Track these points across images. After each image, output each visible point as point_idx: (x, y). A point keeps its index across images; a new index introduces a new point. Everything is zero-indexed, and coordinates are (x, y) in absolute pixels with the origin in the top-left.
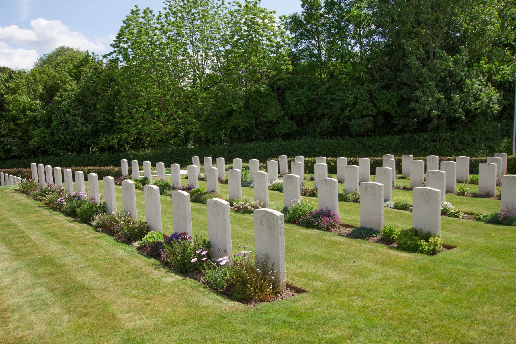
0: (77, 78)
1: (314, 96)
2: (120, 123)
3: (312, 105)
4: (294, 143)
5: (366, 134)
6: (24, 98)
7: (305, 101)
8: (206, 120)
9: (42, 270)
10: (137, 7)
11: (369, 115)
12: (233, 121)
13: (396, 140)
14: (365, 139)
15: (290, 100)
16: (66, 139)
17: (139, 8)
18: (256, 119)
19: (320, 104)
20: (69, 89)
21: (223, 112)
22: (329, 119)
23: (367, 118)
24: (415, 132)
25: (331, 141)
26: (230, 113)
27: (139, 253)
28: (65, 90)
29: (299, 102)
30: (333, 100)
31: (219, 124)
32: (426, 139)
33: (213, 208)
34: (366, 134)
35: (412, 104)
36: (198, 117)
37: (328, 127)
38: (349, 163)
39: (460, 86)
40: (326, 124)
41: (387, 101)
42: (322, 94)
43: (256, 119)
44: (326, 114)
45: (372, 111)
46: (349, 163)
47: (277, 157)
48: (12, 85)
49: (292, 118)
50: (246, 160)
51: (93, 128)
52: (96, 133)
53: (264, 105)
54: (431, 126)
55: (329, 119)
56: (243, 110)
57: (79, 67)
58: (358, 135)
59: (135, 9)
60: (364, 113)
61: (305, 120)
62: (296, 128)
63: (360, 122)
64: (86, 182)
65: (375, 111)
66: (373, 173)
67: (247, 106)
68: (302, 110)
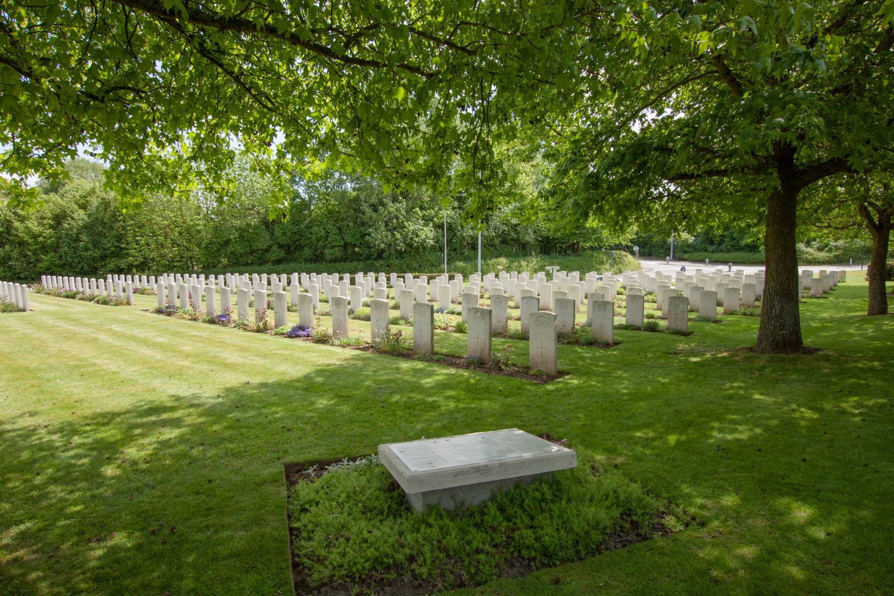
0: (83, 207)
2: (126, 249)
4: (281, 266)
5: (335, 261)
7: (289, 233)
8: (206, 247)
11: (338, 246)
12: (230, 249)
13: (361, 264)
14: (337, 264)
15: (278, 232)
16: (73, 262)
18: (250, 247)
19: (302, 236)
21: (221, 241)
22: (310, 247)
23: (337, 248)
24: (376, 259)
25: (311, 266)
26: (227, 242)
27: (703, 288)
29: (284, 234)
30: (311, 233)
31: (219, 250)
32: (382, 265)
34: (335, 261)
35: (367, 237)
36: (199, 245)
38: (398, 277)
40: (307, 252)
43: (250, 247)
46: (414, 277)
47: (279, 274)
49: (281, 246)
50: (388, 273)
52: (103, 258)
54: (384, 255)
55: (310, 247)
58: (330, 261)
60: (334, 244)
61: (292, 248)
62: (283, 255)
65: (342, 243)
66: (428, 283)
67: (241, 237)
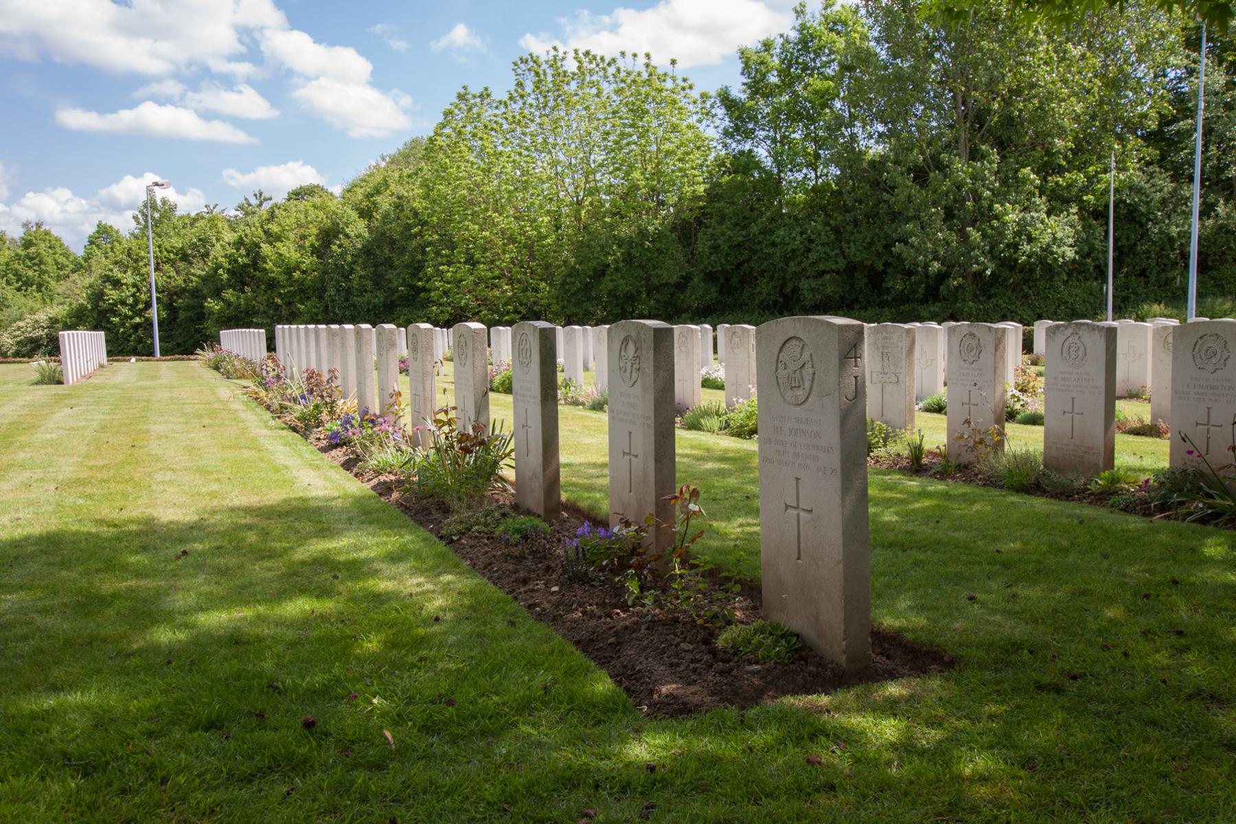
0: (365, 214)
1: (740, 239)
3: (741, 254)
6: (289, 251)
7: (725, 247)
9: (25, 629)
10: (465, 88)
12: (606, 284)
17: (469, 89)
20: (352, 234)
23: (827, 277)
28: (347, 236)
33: (1067, 344)
37: (769, 294)
39: (984, 215)
41: (865, 245)
42: (754, 235)
44: (765, 271)
45: (837, 263)
48: (274, 228)
51: (386, 298)
53: (656, 255)
56: (621, 265)
57: (372, 196)
59: (463, 91)
60: (821, 267)
63: (814, 283)
64: (587, 373)
65: (842, 264)
68: (722, 265)
